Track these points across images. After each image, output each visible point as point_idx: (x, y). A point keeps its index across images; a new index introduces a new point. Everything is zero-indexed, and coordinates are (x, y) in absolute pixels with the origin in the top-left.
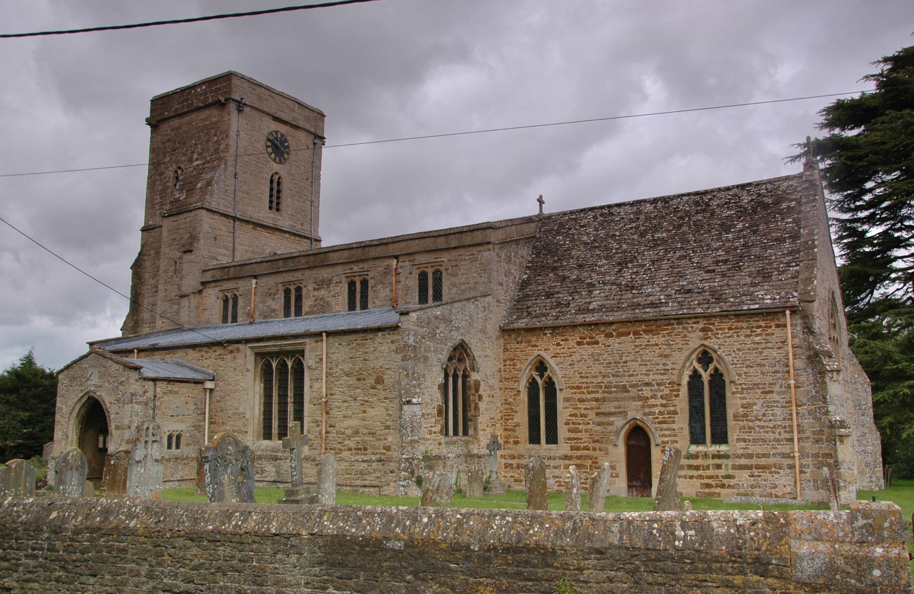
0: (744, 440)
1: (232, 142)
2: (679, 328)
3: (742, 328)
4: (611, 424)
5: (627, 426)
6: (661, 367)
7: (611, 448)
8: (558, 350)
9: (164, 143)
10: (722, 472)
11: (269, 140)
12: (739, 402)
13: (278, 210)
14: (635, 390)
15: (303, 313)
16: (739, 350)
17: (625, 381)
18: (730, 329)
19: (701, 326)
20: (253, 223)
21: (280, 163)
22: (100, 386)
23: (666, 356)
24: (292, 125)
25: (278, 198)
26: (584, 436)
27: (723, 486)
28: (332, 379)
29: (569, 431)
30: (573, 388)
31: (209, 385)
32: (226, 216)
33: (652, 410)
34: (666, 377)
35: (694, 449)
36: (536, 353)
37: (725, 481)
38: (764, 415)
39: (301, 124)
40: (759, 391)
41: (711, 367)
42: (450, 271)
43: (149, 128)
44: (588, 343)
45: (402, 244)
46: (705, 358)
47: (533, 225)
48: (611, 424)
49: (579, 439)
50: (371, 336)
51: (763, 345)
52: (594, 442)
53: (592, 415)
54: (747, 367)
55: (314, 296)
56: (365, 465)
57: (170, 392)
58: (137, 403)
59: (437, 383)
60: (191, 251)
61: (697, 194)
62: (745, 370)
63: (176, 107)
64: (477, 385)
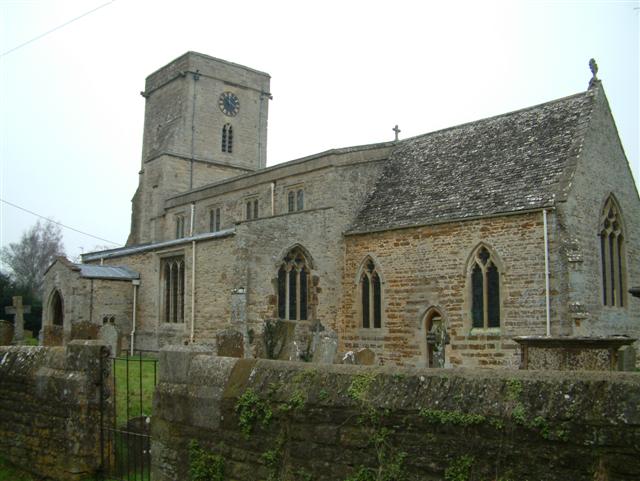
0: (511, 324)
1: (190, 104)
2: (465, 229)
3: (511, 227)
6: (452, 262)
7: (417, 332)
11: (238, 103)
12: (508, 291)
13: (230, 152)
18: (502, 228)
19: (480, 227)
20: (208, 163)
21: (232, 115)
23: (456, 253)
24: (241, 87)
25: (230, 142)
27: (495, 363)
31: (135, 282)
32: (185, 159)
35: (476, 331)
37: (497, 359)
38: (526, 302)
39: (249, 85)
40: (523, 281)
43: (144, 99)
44: (402, 244)
45: (279, 171)
46: (484, 254)
47: (387, 150)
48: (417, 311)
50: (219, 242)
53: (404, 304)
57: (105, 287)
59: (270, 278)
61: (508, 115)
62: (513, 263)
63: (160, 82)
64: (316, 280)
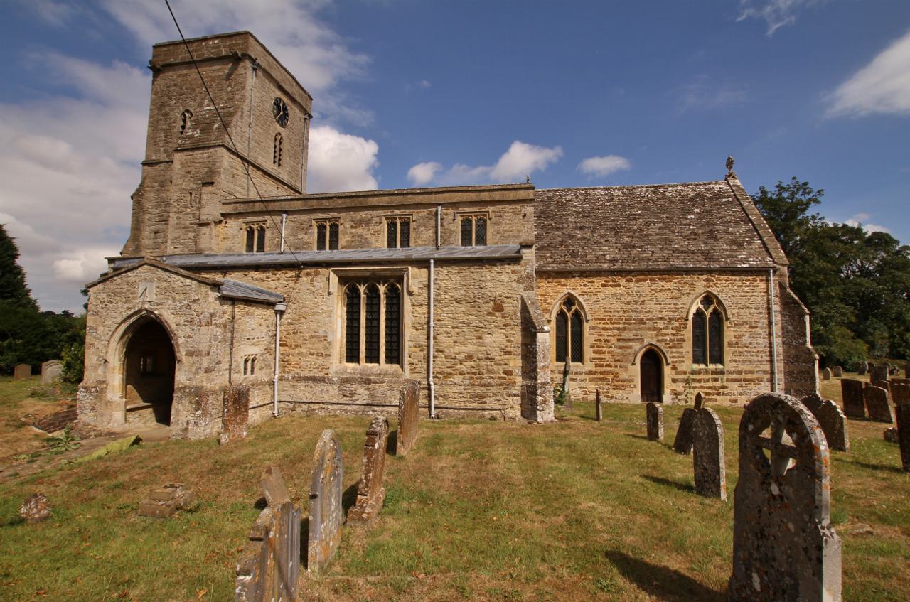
0: (736, 361)
4: (630, 347)
5: (644, 350)
6: (672, 306)
8: (585, 289)
9: (169, 87)
10: (718, 384)
12: (732, 333)
14: (651, 323)
15: (340, 246)
16: (733, 296)
17: (642, 315)
22: (161, 304)
23: (677, 298)
25: (280, 155)
26: (607, 356)
27: (719, 394)
28: (440, 306)
29: (594, 352)
30: (598, 319)
31: (280, 307)
33: (665, 338)
34: (676, 314)
35: (696, 367)
36: (566, 291)
37: (721, 391)
38: (751, 343)
40: (747, 326)
41: (574, 308)
42: (493, 220)
44: (611, 286)
46: (708, 299)
48: (630, 347)
49: (602, 358)
51: (751, 294)
52: (615, 361)
53: (614, 341)
54: (739, 308)
55: (351, 233)
56: (483, 388)
58: (216, 325)
60: (212, 184)
